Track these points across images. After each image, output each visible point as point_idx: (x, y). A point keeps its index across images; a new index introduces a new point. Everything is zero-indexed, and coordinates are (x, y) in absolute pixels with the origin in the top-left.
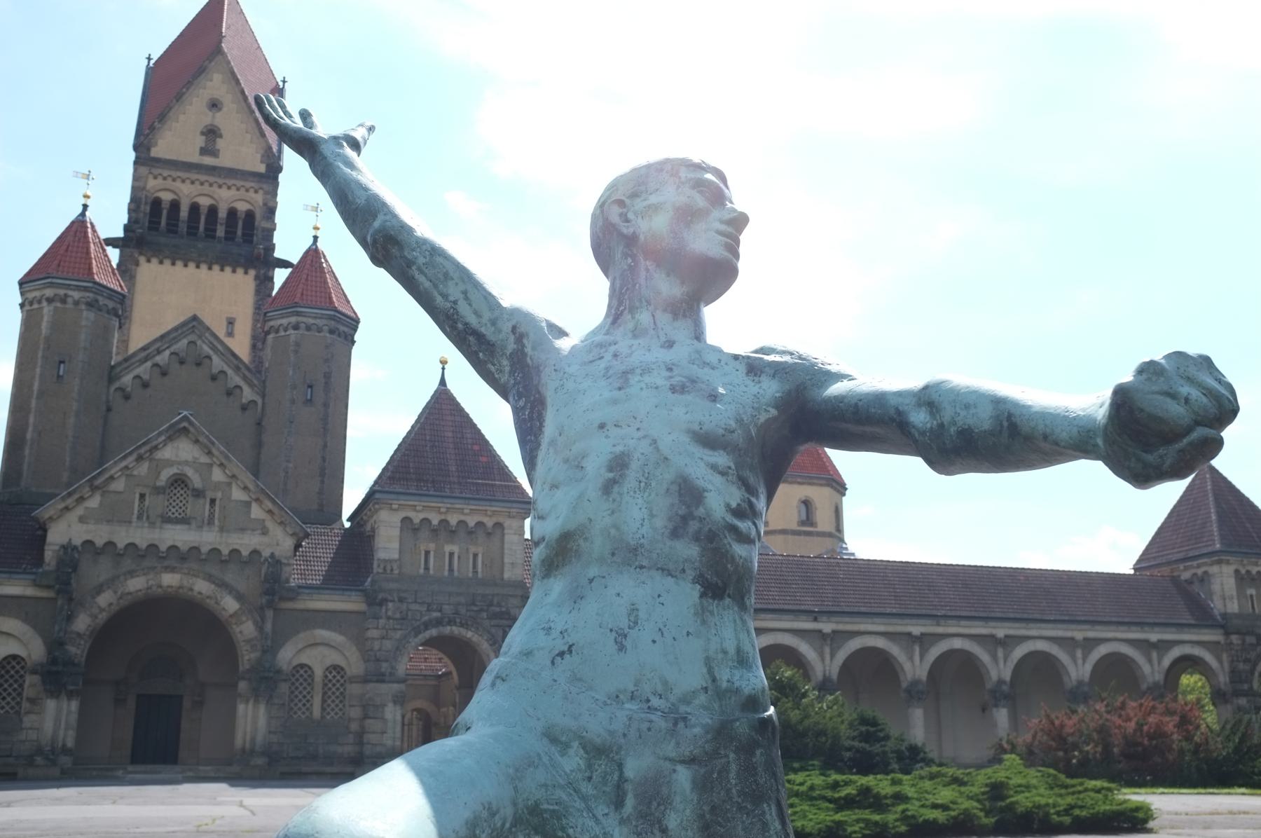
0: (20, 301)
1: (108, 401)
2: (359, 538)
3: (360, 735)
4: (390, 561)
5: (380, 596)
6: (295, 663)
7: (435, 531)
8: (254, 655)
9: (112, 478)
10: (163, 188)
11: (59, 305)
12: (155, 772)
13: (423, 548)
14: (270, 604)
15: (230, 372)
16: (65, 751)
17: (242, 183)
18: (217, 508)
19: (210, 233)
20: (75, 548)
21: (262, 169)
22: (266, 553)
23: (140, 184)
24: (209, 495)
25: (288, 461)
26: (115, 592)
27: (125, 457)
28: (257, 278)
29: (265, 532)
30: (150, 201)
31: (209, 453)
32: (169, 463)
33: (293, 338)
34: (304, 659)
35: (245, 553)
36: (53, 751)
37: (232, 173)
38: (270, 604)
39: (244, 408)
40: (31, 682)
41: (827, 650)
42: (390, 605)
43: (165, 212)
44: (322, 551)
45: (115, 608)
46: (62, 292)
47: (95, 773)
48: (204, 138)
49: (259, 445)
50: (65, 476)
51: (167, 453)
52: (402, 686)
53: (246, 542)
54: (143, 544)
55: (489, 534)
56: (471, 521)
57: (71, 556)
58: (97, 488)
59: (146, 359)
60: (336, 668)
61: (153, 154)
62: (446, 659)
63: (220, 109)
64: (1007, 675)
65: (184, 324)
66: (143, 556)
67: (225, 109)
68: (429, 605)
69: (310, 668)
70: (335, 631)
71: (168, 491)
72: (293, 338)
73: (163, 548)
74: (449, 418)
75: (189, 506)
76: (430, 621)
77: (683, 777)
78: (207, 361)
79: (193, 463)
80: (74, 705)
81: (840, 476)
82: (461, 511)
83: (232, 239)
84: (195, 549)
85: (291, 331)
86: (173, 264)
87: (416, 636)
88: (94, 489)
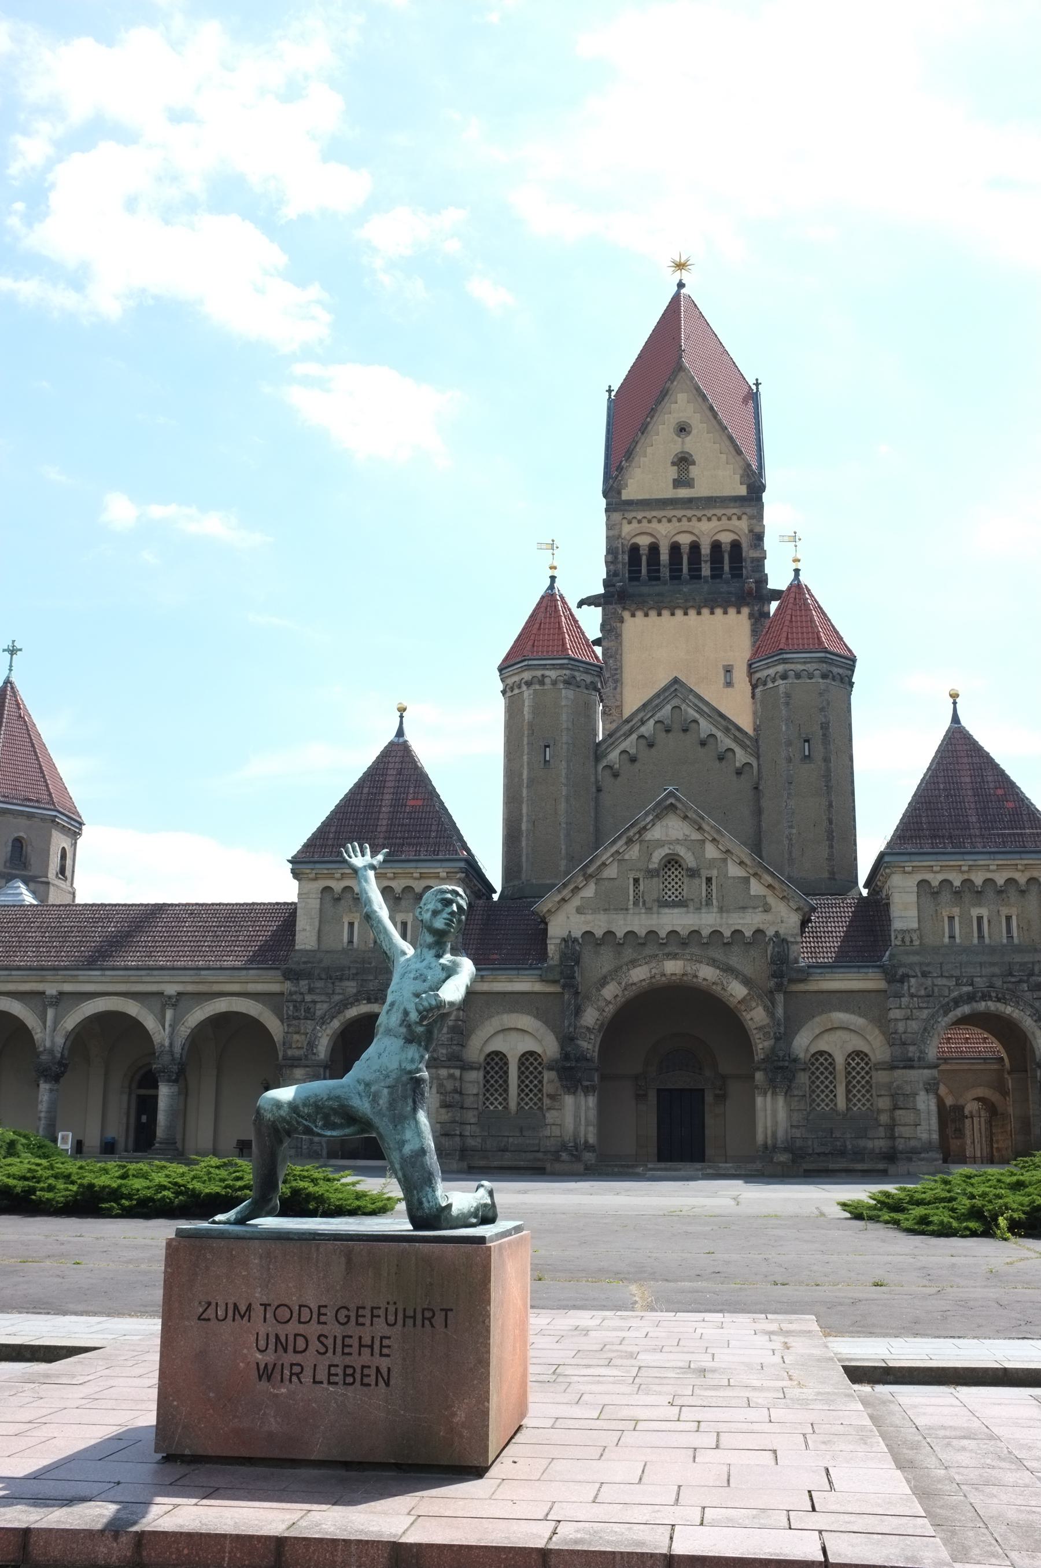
0: (501, 687)
1: (597, 781)
2: (873, 914)
3: (891, 1127)
4: (909, 931)
5: (901, 971)
6: (813, 1050)
7: (958, 894)
8: (768, 1044)
9: (604, 864)
10: (641, 533)
11: (537, 687)
12: (676, 1170)
13: (945, 914)
14: (779, 987)
15: (719, 734)
16: (588, 1147)
17: (723, 511)
18: (714, 887)
19: (695, 574)
20: (575, 940)
21: (743, 491)
22: (770, 932)
23: (615, 532)
24: (705, 873)
25: (791, 827)
26: (620, 984)
27: (614, 842)
28: (751, 616)
29: (767, 909)
30: (626, 549)
31: (700, 829)
32: (660, 843)
33: (782, 689)
34: (822, 1045)
35: (748, 934)
36: (576, 1147)
38: (779, 987)
39: (739, 773)
42: (913, 980)
43: (644, 559)
44: (834, 922)
45: (621, 1000)
46: (539, 673)
47: (616, 1170)
48: (676, 468)
49: (758, 812)
50: (563, 864)
51: (656, 833)
52: (935, 1072)
53: (749, 922)
55: (1023, 892)
56: (1000, 879)
57: (573, 950)
58: (591, 876)
59: (631, 732)
60: (858, 1053)
61: (624, 498)
62: (992, 1039)
63: (689, 433)
65: (665, 689)
66: (644, 944)
67: (694, 432)
68: (958, 978)
69: (830, 1055)
70: (853, 1013)
71: (662, 873)
72: (782, 689)
73: (663, 934)
74: (965, 760)
75: (685, 887)
76: (961, 996)
77: (386, 1091)
78: (694, 725)
79: (685, 841)
80: (592, 1101)
83: (720, 576)
84: (695, 933)
85: (780, 682)
86: (659, 615)
87: (946, 1014)
88: (588, 878)
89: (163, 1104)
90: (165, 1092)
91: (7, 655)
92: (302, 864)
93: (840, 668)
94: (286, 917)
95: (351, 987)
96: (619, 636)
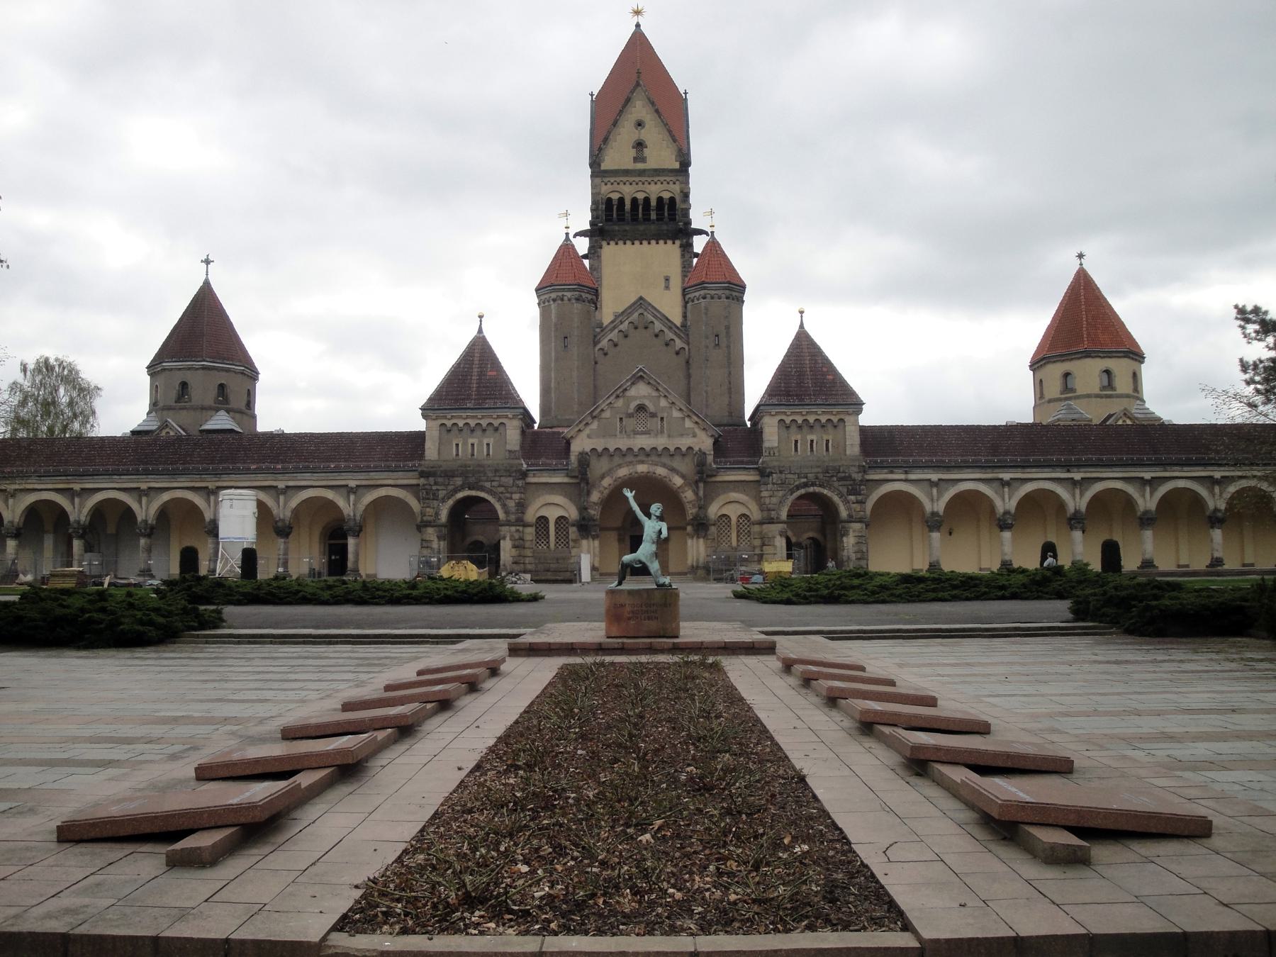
7: (800, 427)
8: (694, 511)
14: (701, 480)
19: (647, 219)
21: (677, 166)
22: (696, 449)
24: (660, 415)
32: (635, 398)
34: (724, 511)
35: (684, 449)
37: (658, 172)
38: (701, 480)
39: (677, 353)
40: (573, 532)
41: (1077, 491)
49: (689, 376)
51: (633, 392)
53: (684, 443)
54: (624, 448)
56: (823, 419)
57: (584, 460)
59: (614, 328)
60: (744, 515)
64: (1222, 506)
77: (421, 591)
81: (1138, 346)
82: (816, 413)
88: (594, 418)
89: (351, 548)
90: (351, 542)
91: (204, 265)
92: (428, 410)
93: (735, 290)
94: (414, 441)
95: (459, 481)
96: (599, 257)
